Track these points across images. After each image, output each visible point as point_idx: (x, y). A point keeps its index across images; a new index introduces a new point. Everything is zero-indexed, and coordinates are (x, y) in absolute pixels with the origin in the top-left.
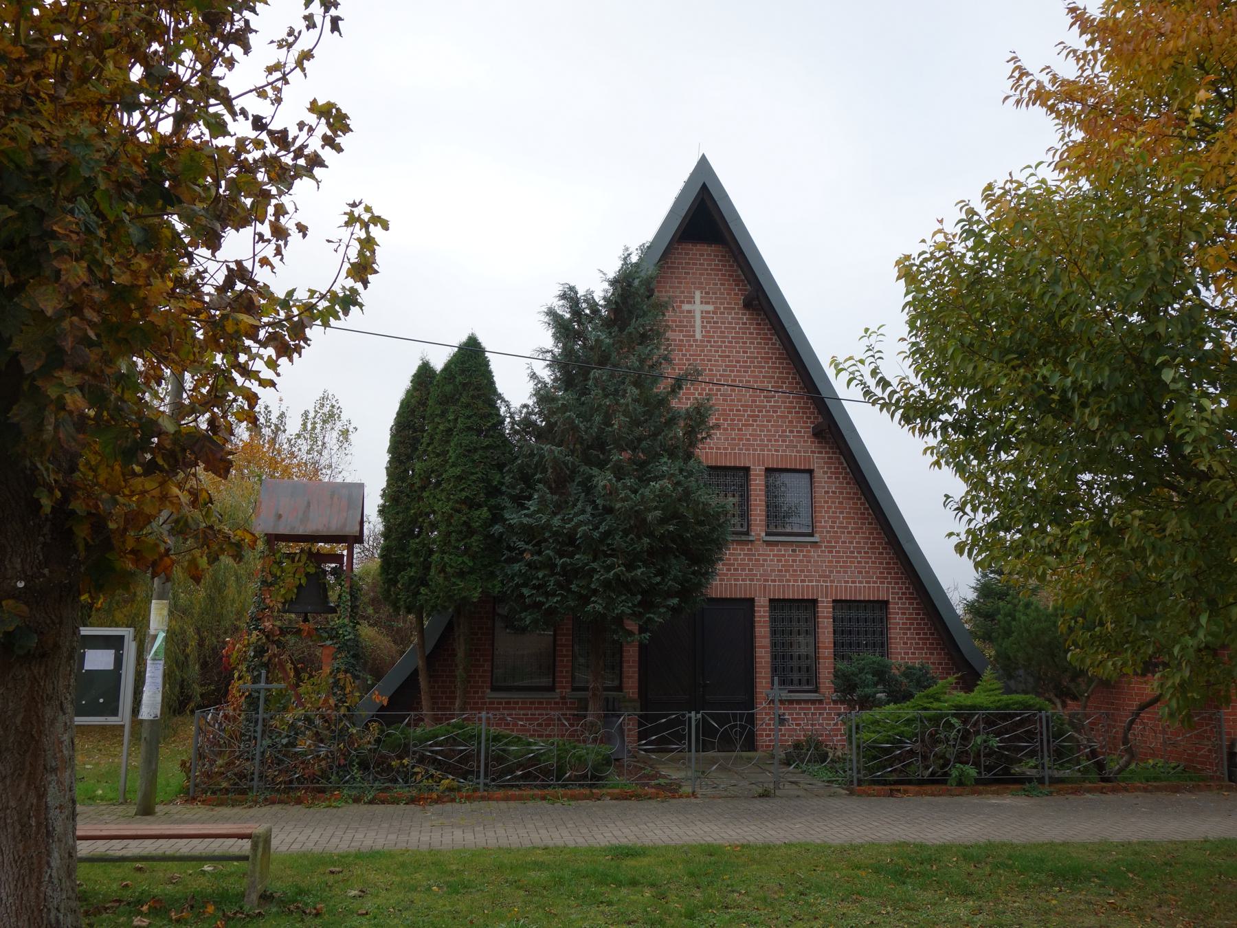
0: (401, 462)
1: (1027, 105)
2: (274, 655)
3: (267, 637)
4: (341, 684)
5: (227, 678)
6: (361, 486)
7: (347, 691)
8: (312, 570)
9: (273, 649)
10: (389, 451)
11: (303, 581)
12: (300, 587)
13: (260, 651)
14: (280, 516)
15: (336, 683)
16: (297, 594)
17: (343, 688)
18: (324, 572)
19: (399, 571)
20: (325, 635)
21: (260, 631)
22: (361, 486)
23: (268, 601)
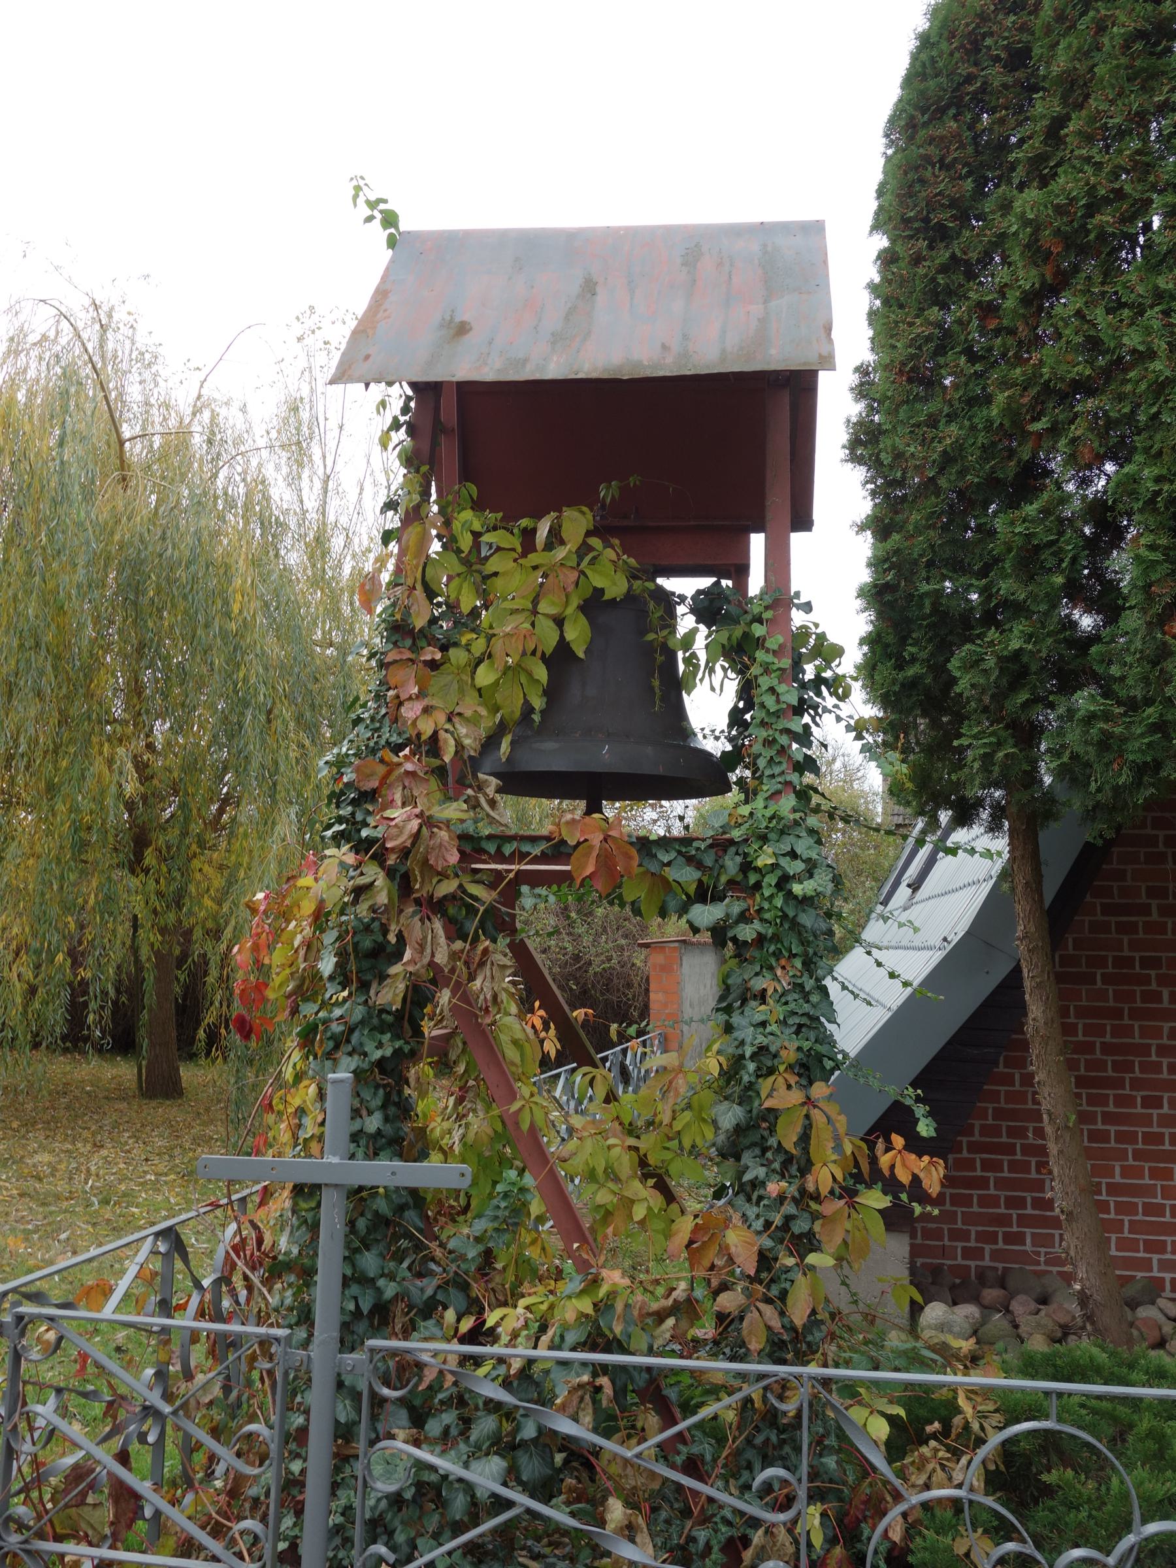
0: (939, 235)
1: (817, 725)
2: (437, 976)
3: (403, 884)
4: (788, 1135)
5: (633, 911)
6: (815, 229)
7: (824, 1176)
8: (615, 586)
9: (429, 944)
10: (880, 193)
11: (577, 633)
12: (560, 659)
13: (368, 957)
14: (462, 329)
15: (752, 1134)
16: (552, 692)
17: (797, 1164)
18: (668, 601)
19: (945, 648)
20: (687, 876)
21: (361, 846)
22: (815, 229)
23: (410, 711)
